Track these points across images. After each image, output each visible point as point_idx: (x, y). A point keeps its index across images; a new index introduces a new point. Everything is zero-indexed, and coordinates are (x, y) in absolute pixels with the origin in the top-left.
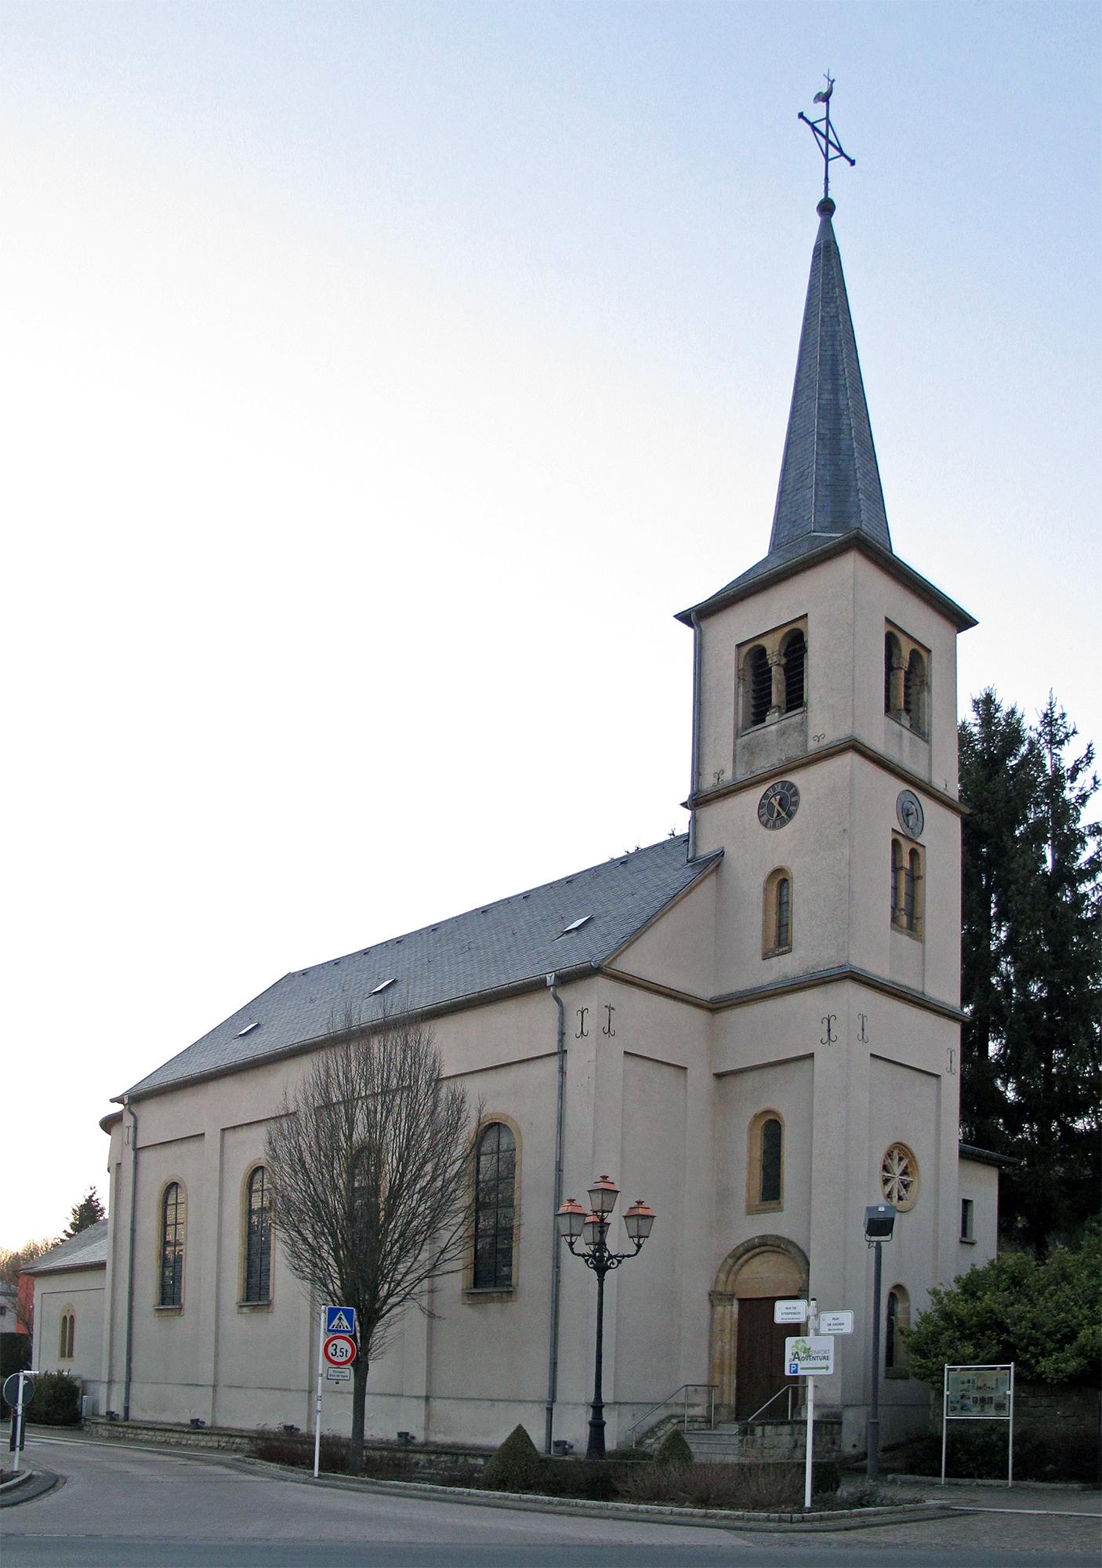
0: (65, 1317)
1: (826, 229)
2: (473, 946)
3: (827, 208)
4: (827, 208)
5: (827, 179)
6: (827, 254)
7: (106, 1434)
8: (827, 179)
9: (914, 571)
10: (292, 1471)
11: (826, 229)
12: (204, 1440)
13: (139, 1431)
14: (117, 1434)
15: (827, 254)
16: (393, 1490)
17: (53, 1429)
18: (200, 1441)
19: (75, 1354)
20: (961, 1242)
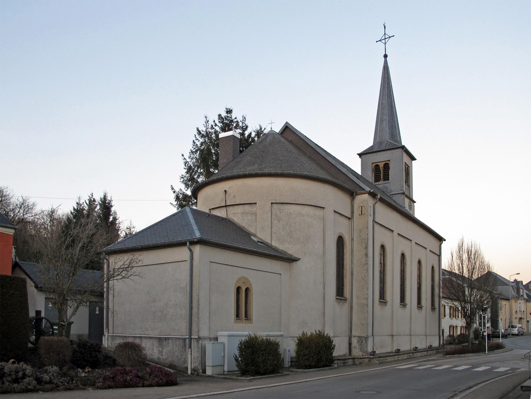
0: (377, 166)
1: (386, 63)
2: (288, 236)
3: (386, 56)
4: (386, 56)
5: (385, 49)
6: (386, 68)
7: (377, 362)
8: (385, 49)
9: (267, 258)
10: (479, 354)
11: (386, 63)
12: (419, 354)
13: (387, 358)
14: (381, 361)
15: (386, 68)
16: (498, 352)
17: (323, 370)
18: (403, 357)
19: (393, 230)
20: (418, 307)
